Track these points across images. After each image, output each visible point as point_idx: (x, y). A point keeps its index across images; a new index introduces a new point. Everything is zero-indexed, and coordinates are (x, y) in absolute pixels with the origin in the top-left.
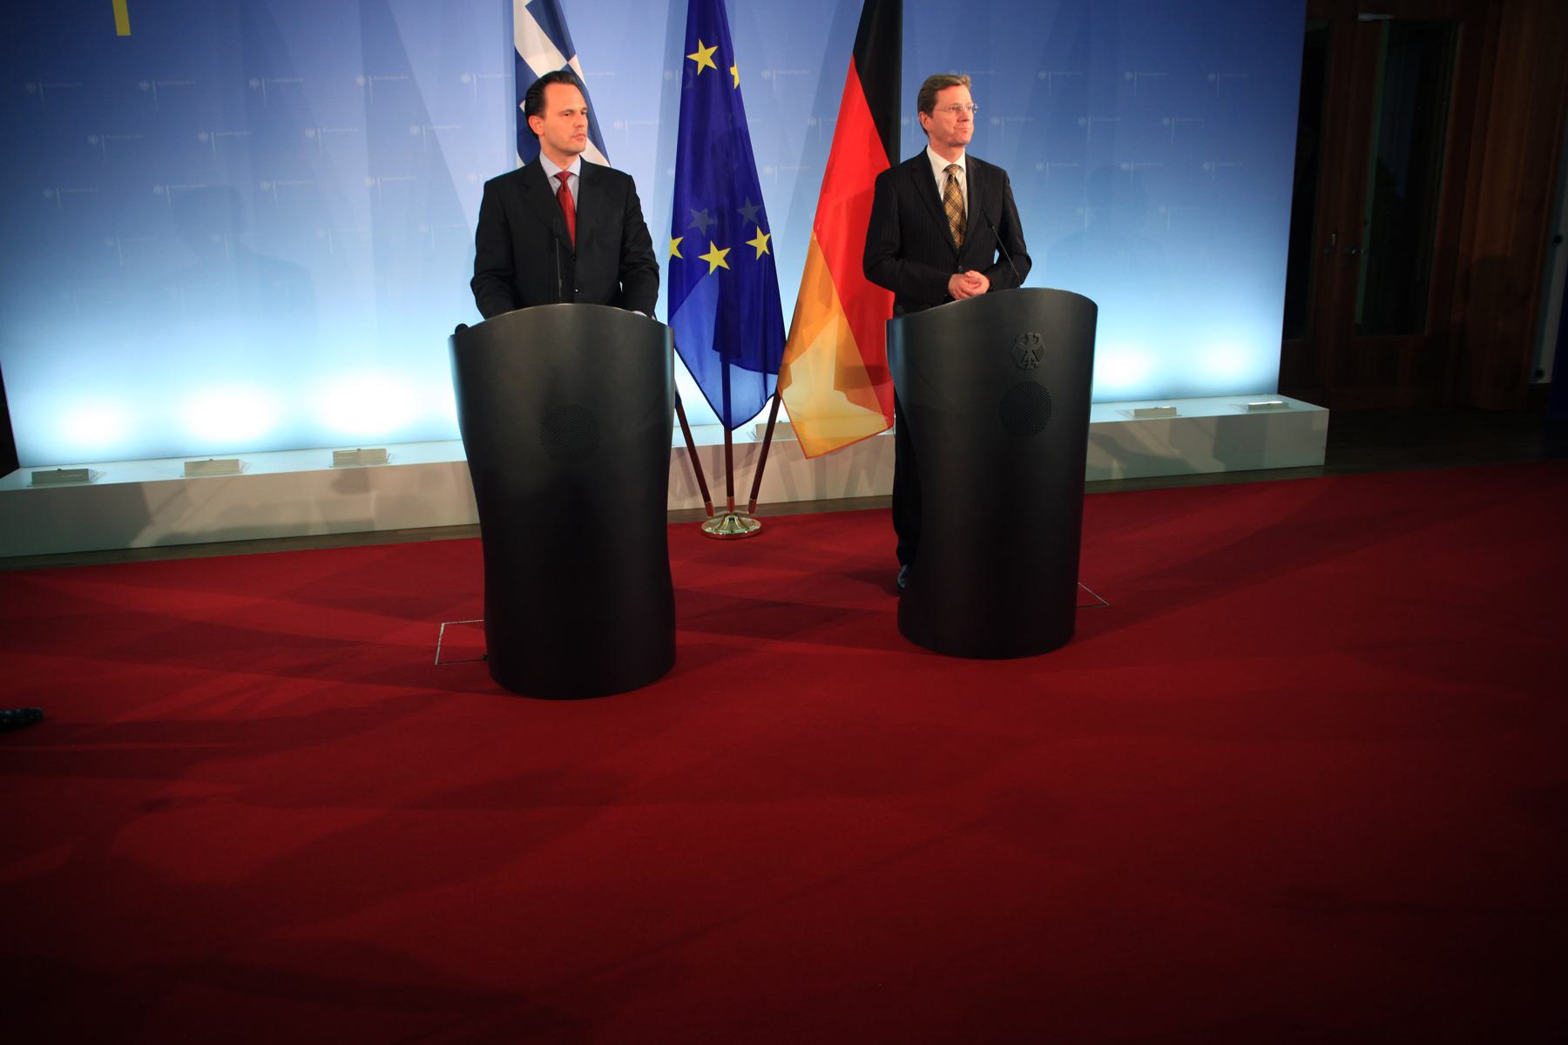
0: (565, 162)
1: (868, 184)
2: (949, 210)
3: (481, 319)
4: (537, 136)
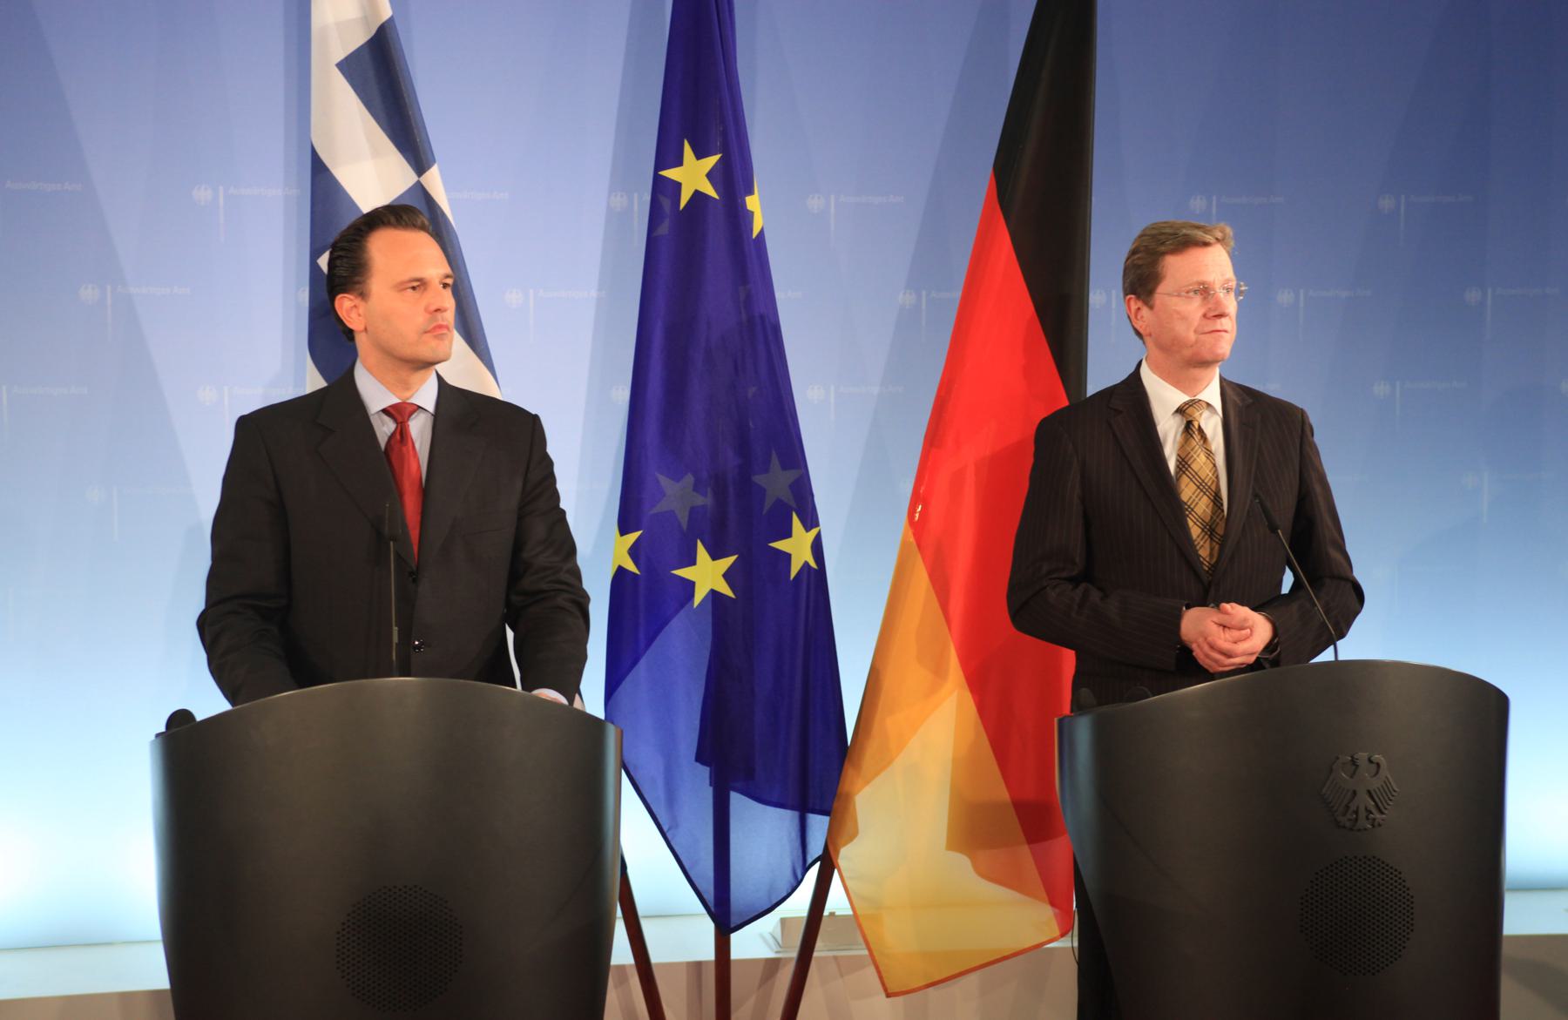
0: (406, 386)
1: (1021, 430)
2: (1187, 491)
4: (350, 334)
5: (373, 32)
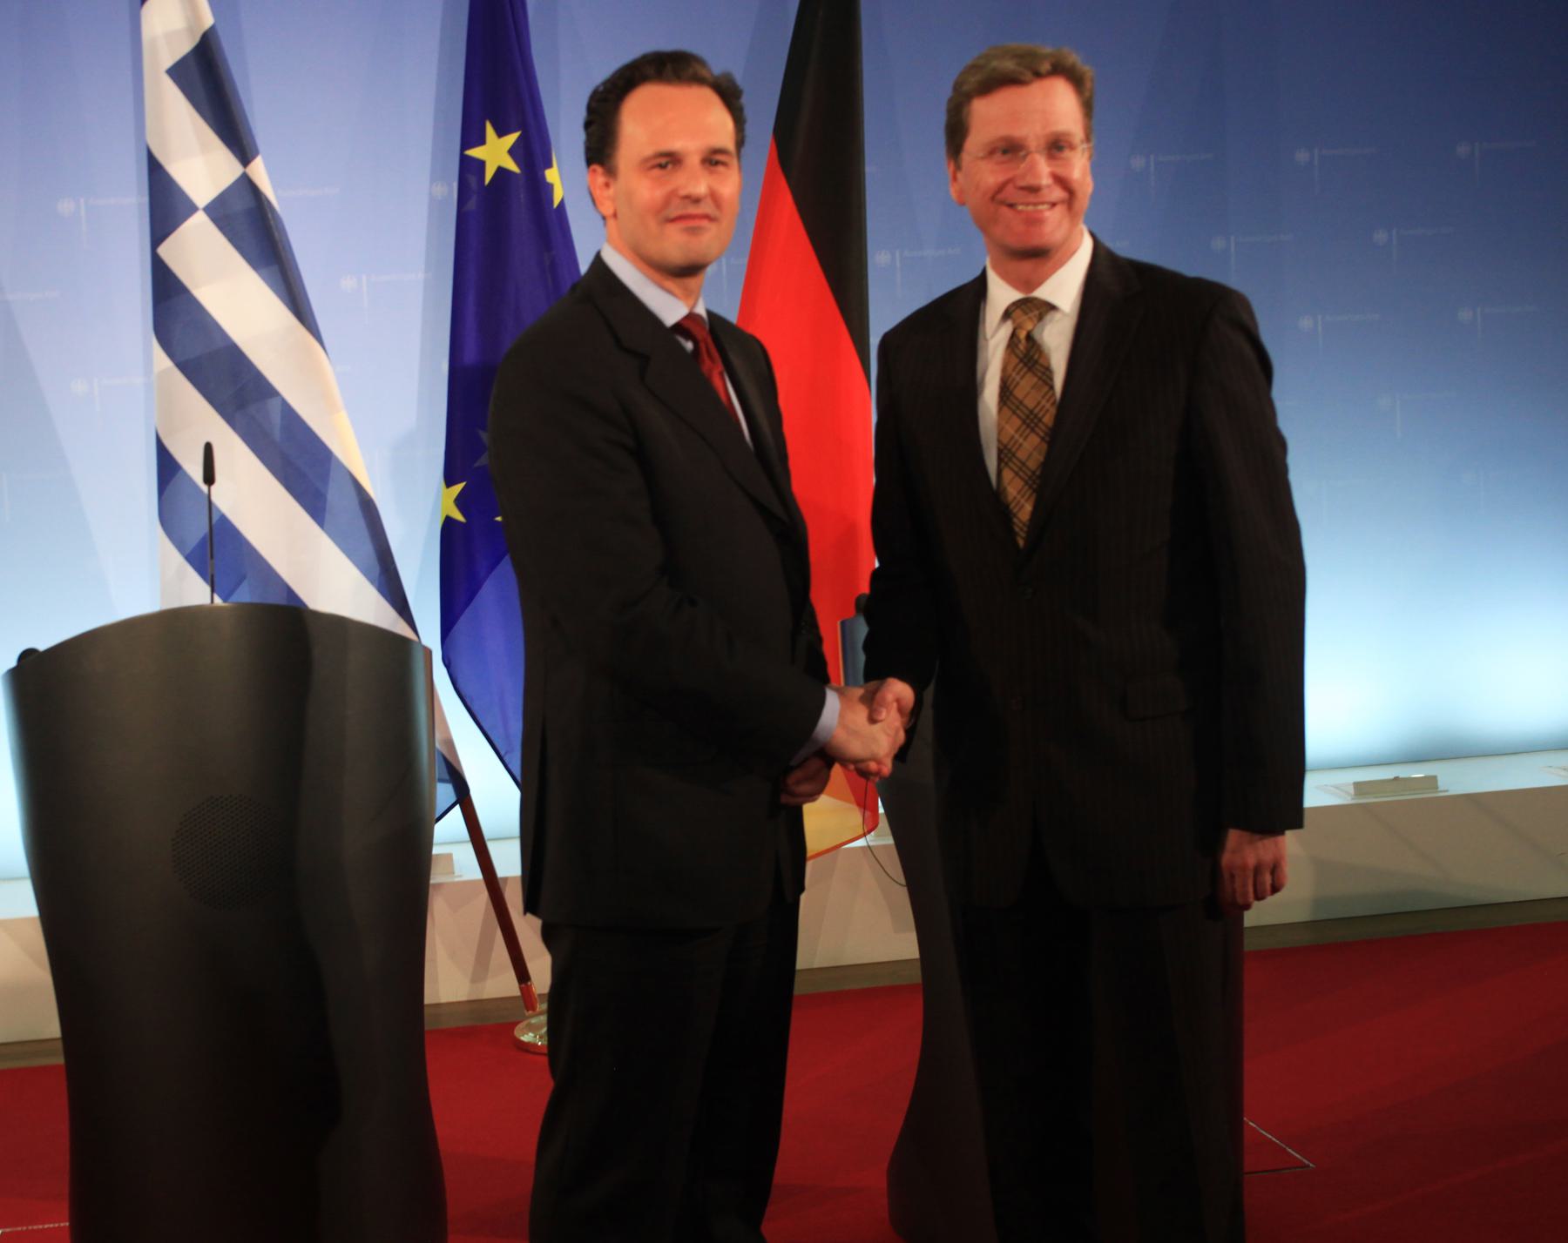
5: (197, 39)
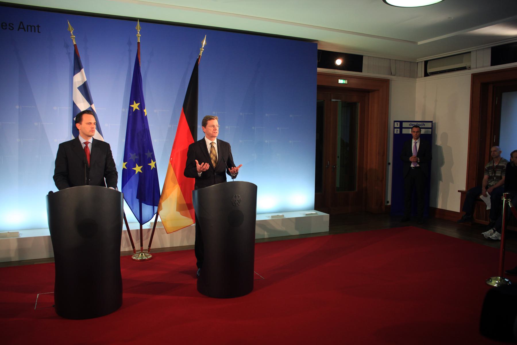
1: (187, 147)
2: (212, 156)
3: (58, 190)
4: (78, 130)
